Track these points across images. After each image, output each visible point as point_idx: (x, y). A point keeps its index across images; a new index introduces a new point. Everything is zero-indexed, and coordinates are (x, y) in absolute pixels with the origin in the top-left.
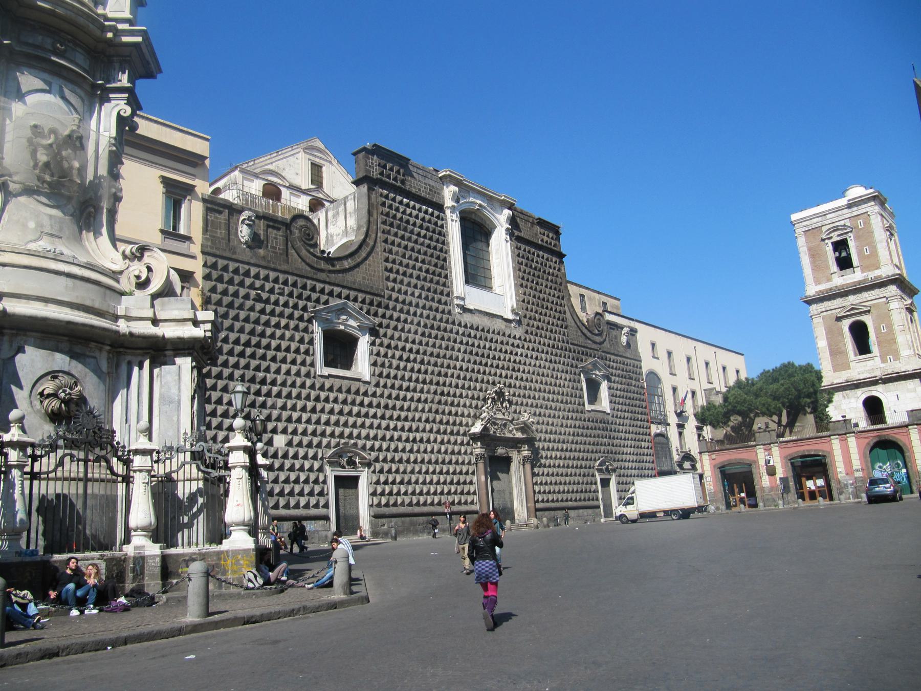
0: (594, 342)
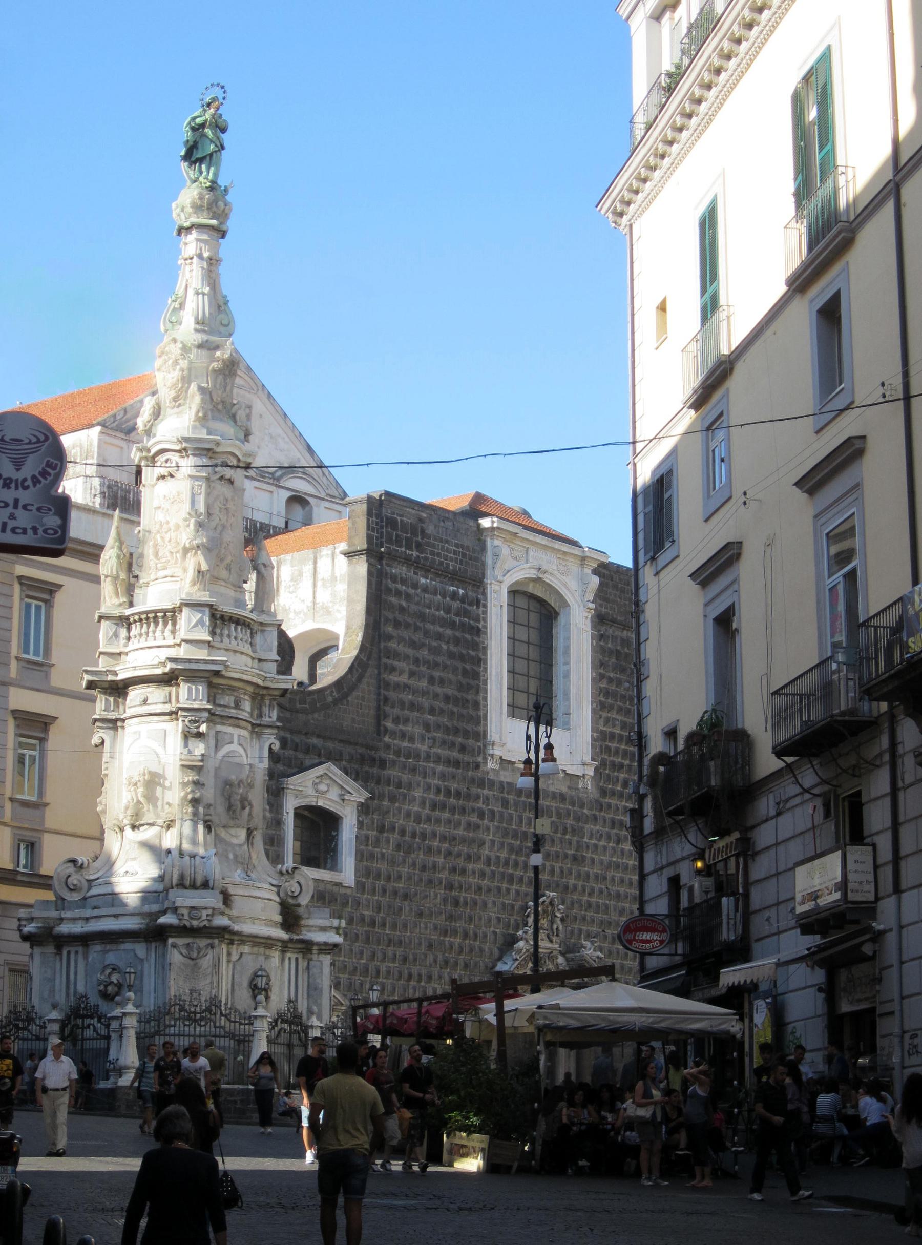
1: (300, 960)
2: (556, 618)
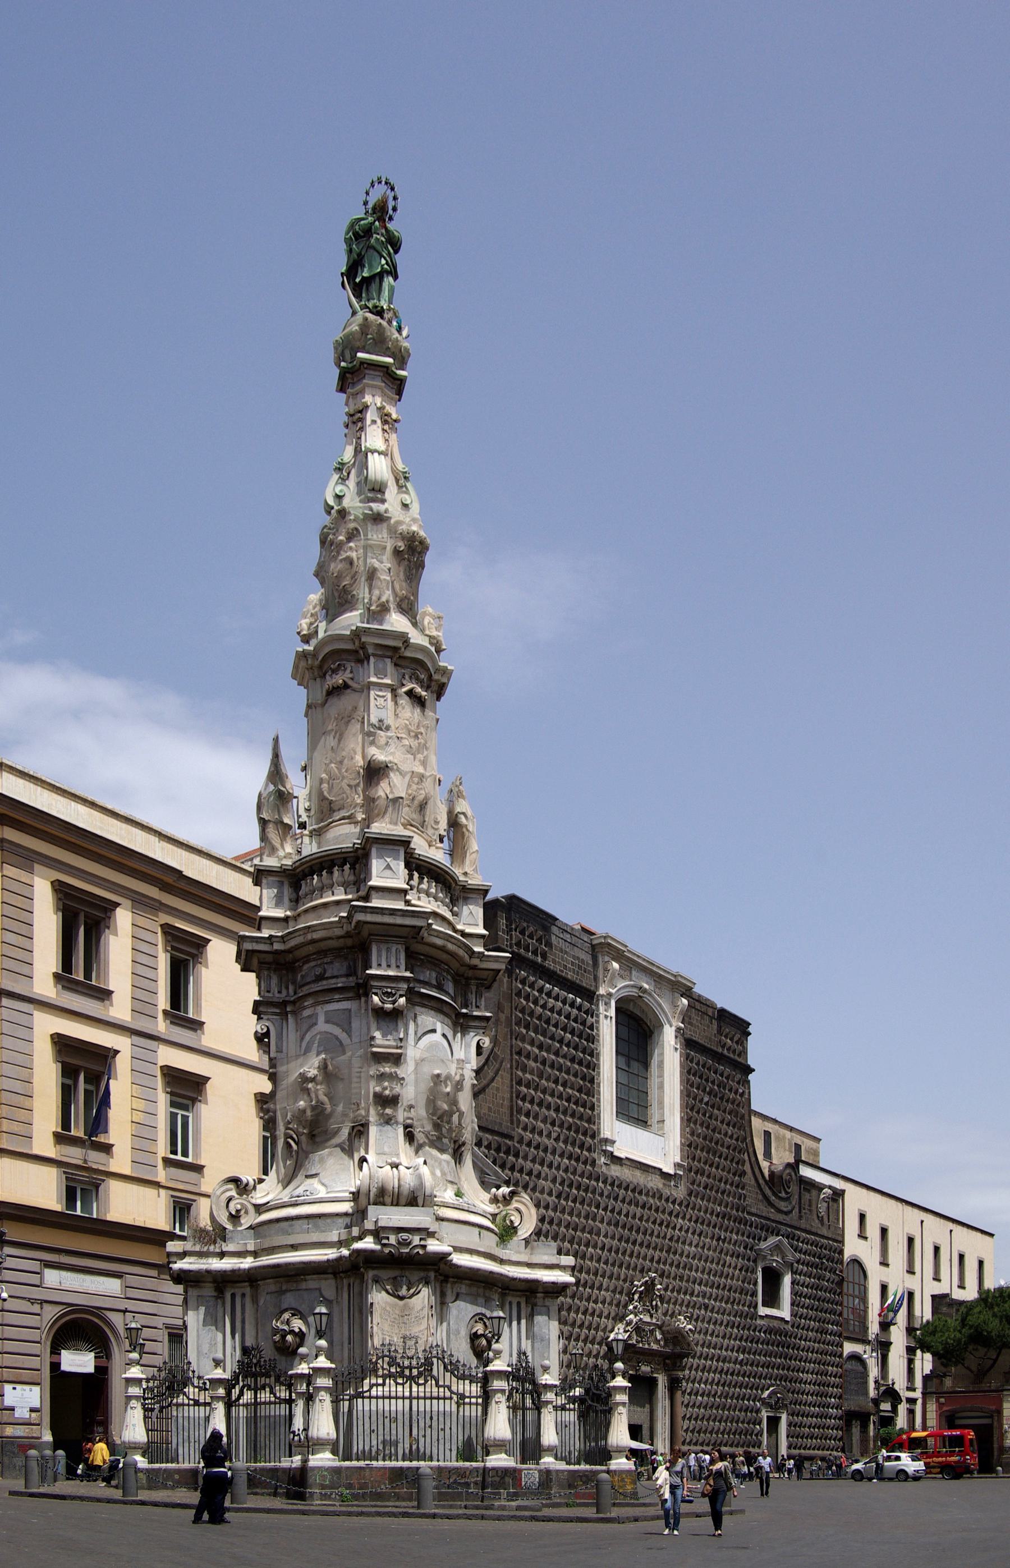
0: (779, 1211)
1: (523, 1305)
2: (651, 1036)
